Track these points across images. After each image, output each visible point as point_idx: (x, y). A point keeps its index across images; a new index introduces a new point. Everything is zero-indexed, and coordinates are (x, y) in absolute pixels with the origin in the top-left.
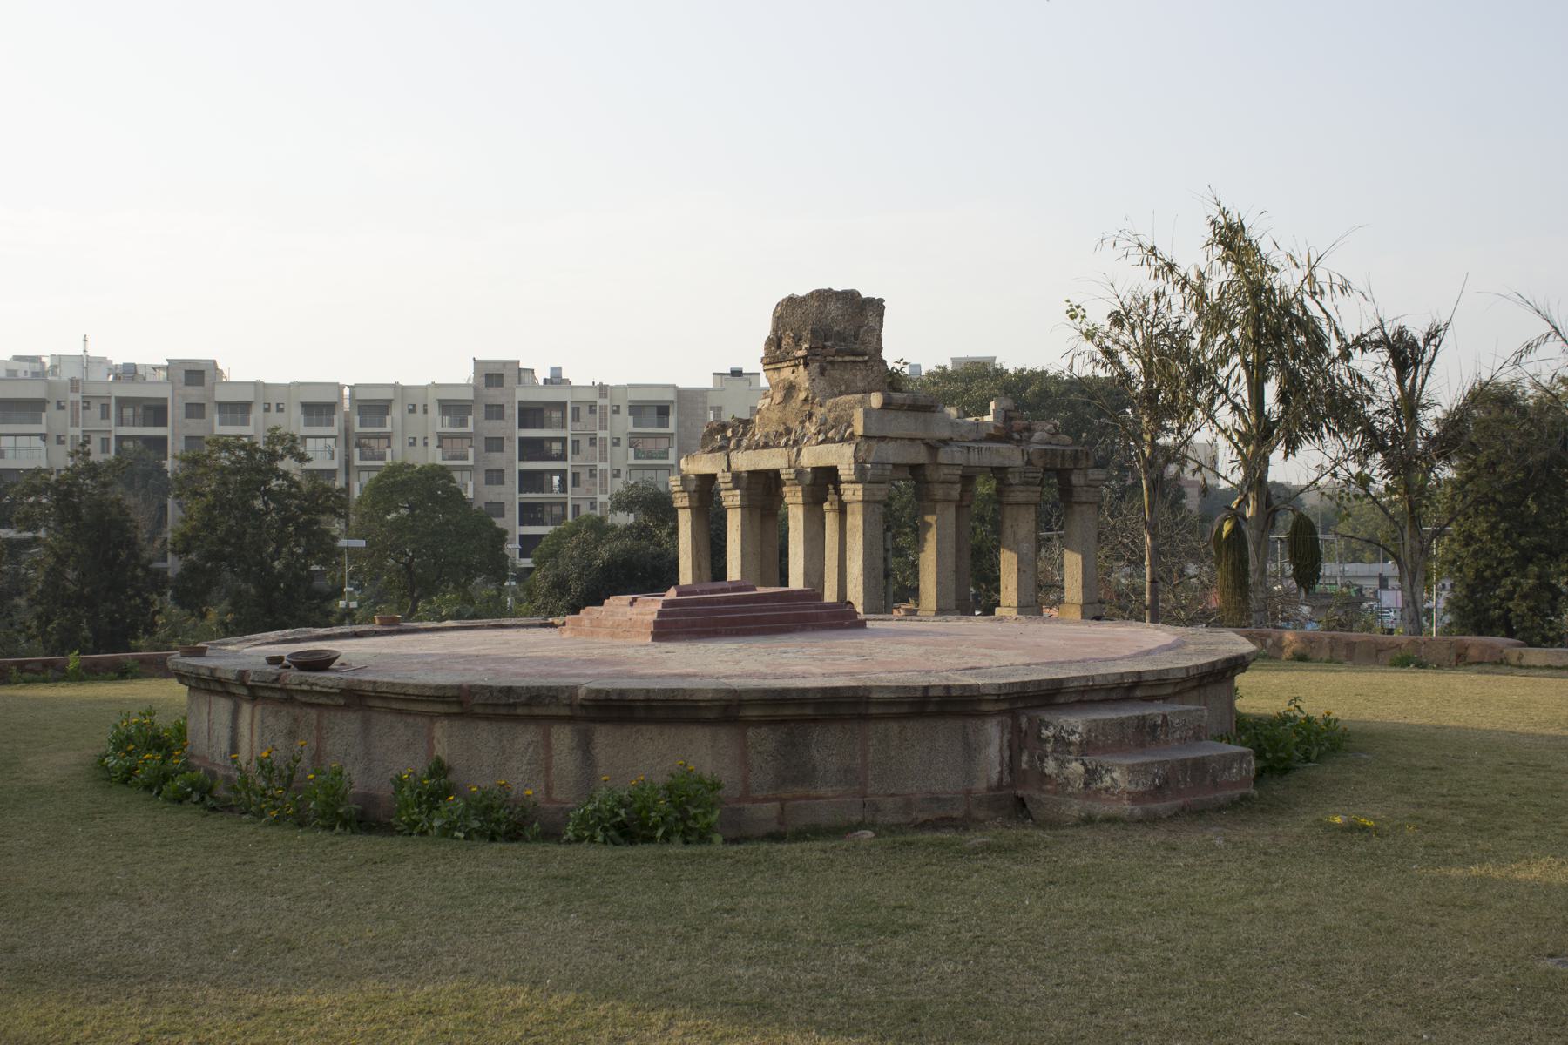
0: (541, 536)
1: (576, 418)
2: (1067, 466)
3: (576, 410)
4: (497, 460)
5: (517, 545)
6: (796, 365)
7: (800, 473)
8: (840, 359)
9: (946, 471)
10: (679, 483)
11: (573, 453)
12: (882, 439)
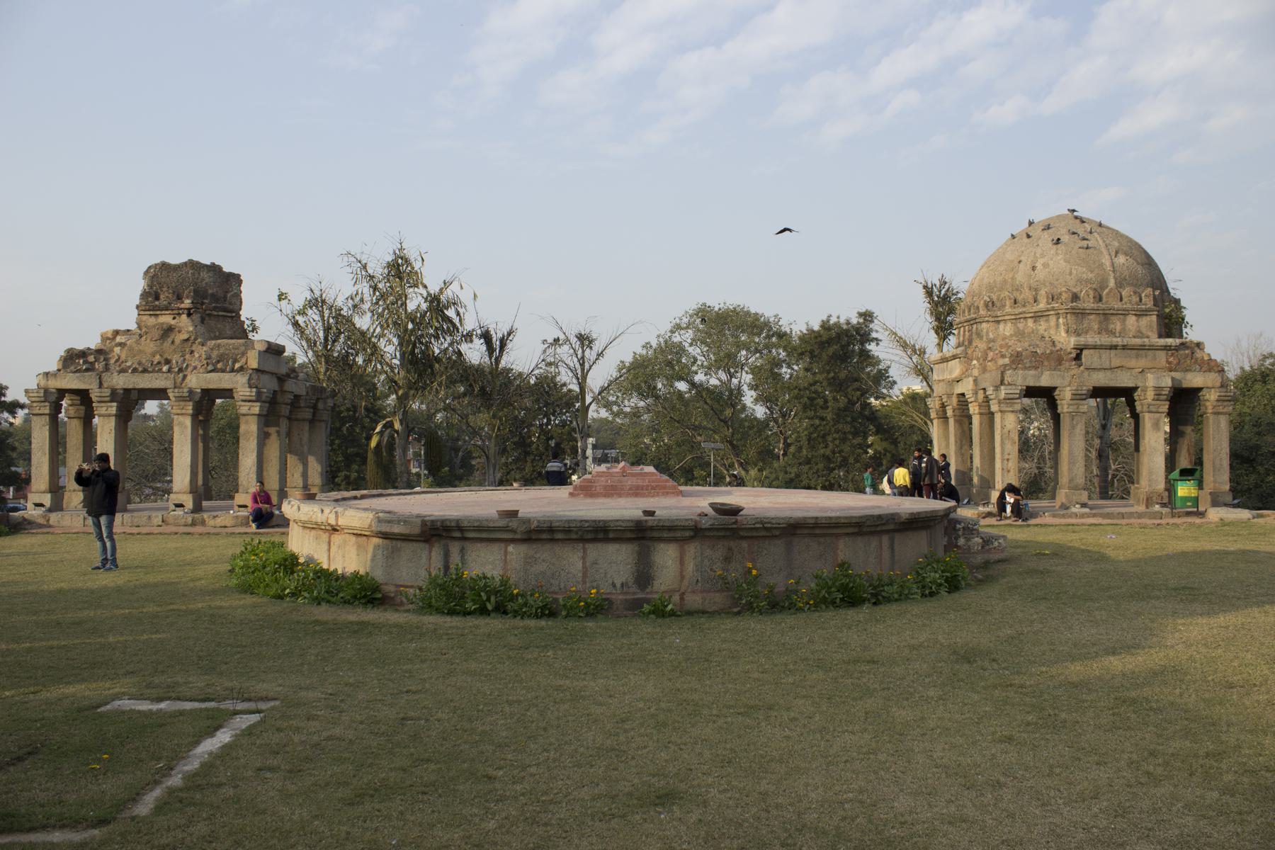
6: (179, 314)
10: (42, 395)
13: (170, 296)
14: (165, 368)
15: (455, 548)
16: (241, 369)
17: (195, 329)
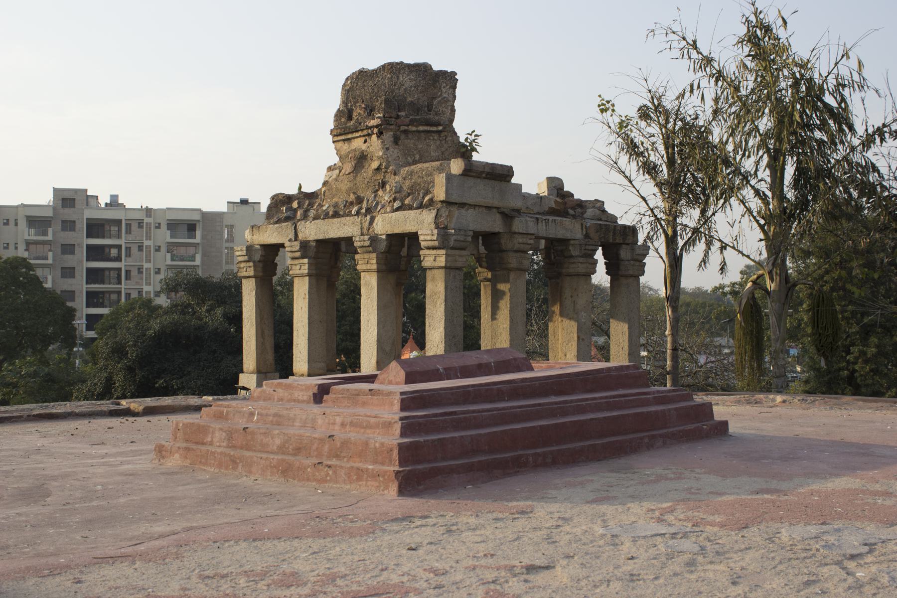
0: (101, 316)
1: (129, 231)
2: (617, 241)
3: (128, 226)
4: (70, 261)
5: (84, 321)
6: (369, 135)
7: (374, 239)
8: (414, 129)
9: (521, 240)
10: (244, 253)
11: (126, 256)
12: (462, 205)
13: (362, 112)
16: (431, 202)
17: (385, 153)
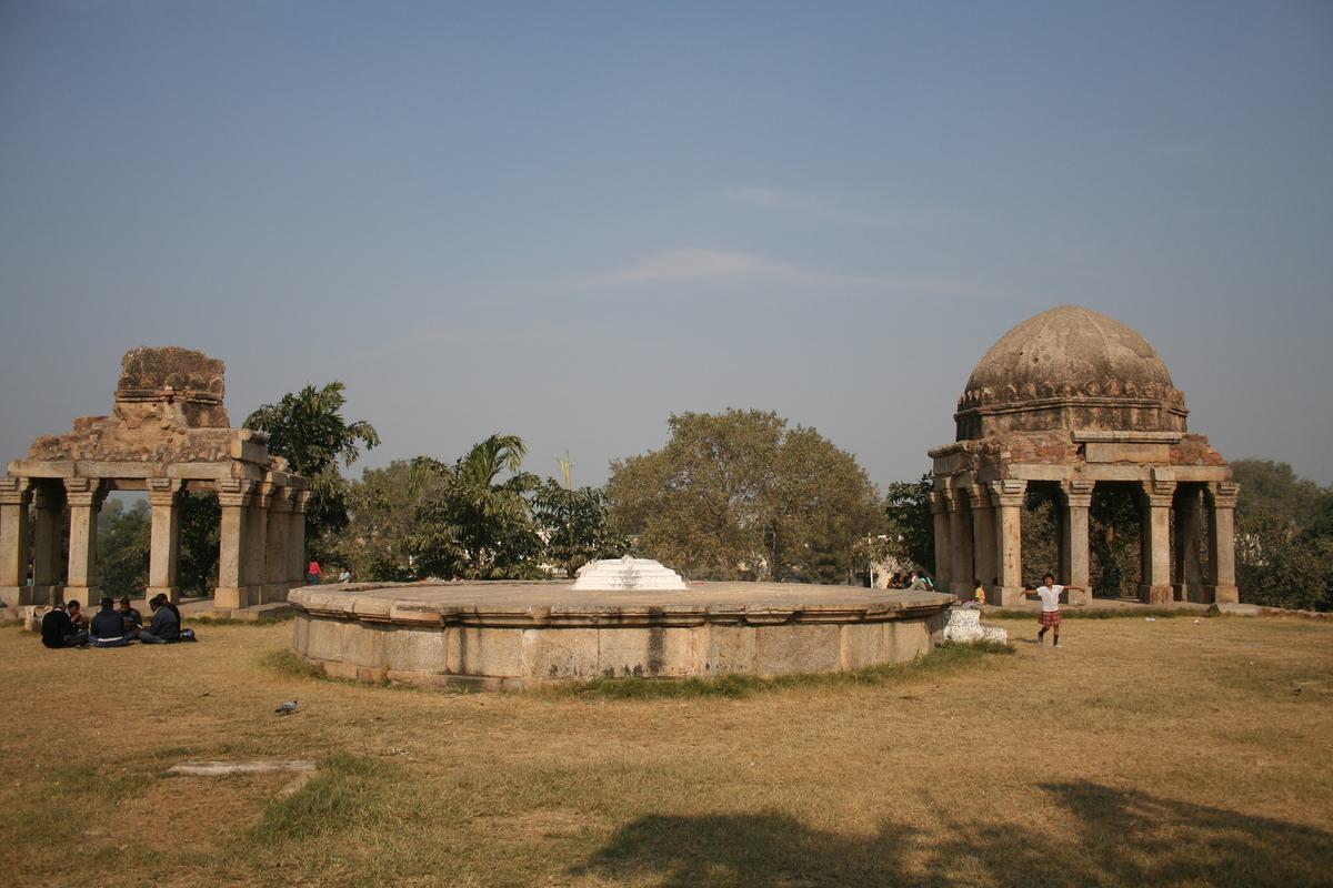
14: (145, 457)
15: (472, 633)
